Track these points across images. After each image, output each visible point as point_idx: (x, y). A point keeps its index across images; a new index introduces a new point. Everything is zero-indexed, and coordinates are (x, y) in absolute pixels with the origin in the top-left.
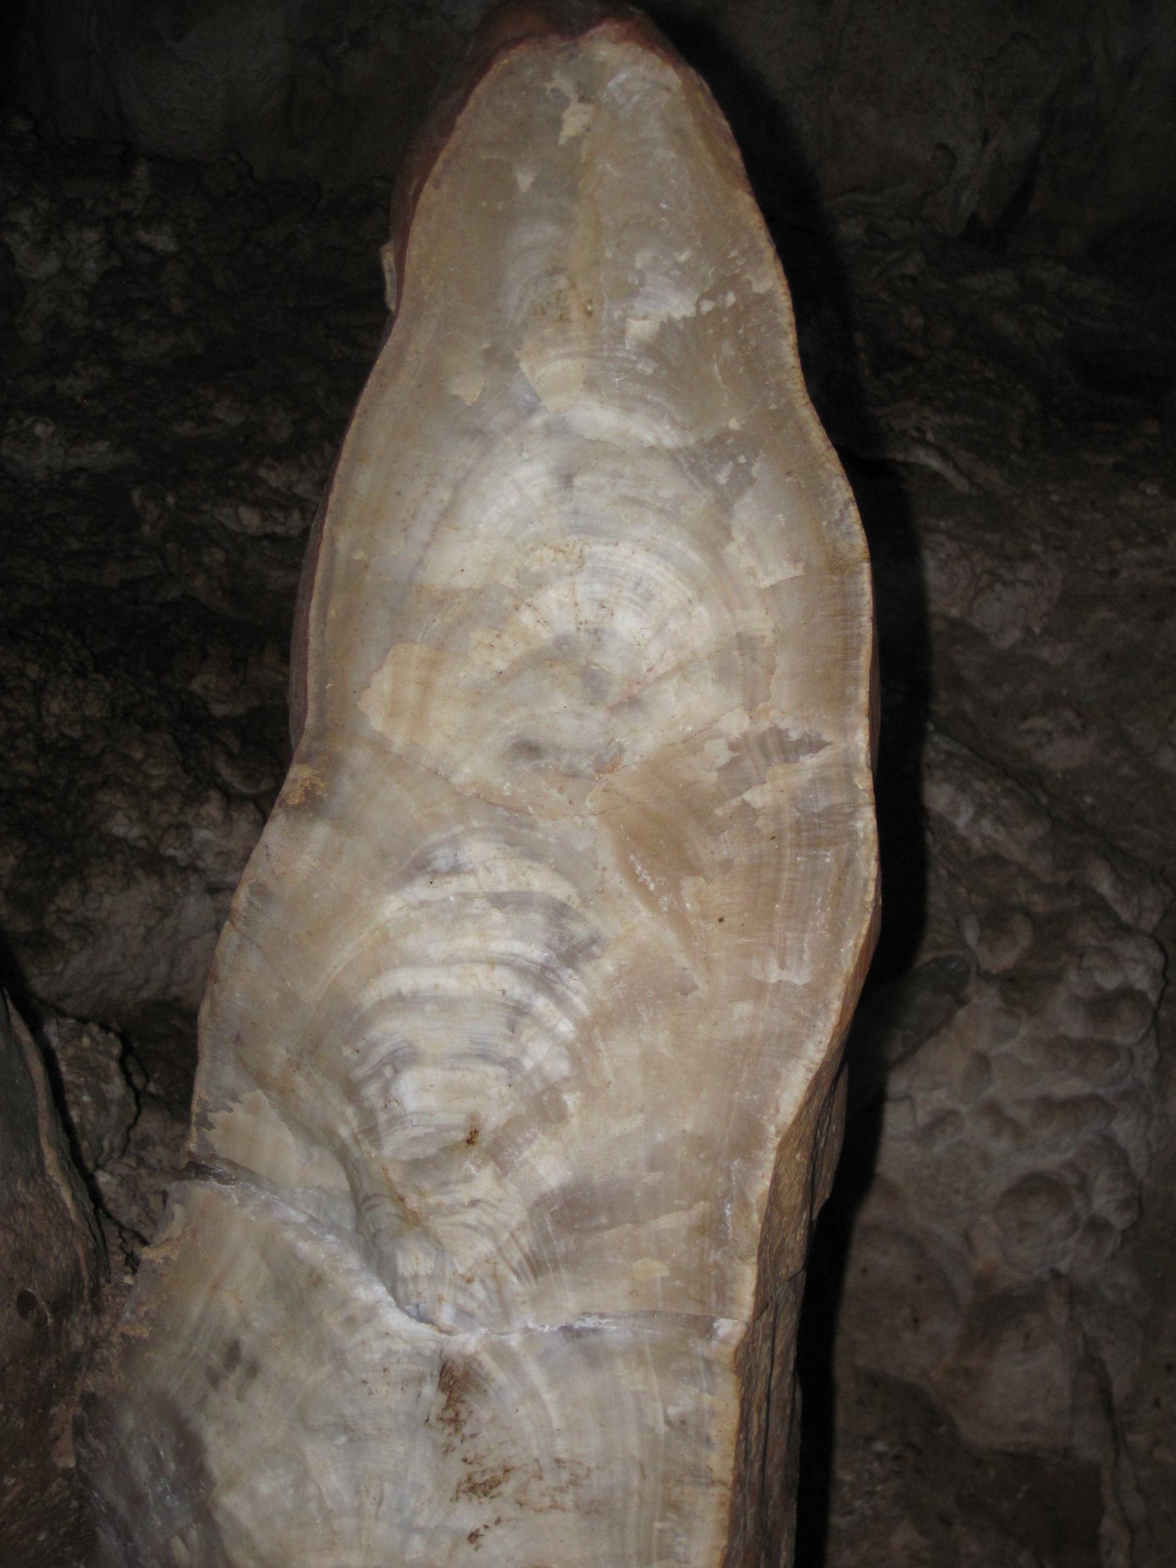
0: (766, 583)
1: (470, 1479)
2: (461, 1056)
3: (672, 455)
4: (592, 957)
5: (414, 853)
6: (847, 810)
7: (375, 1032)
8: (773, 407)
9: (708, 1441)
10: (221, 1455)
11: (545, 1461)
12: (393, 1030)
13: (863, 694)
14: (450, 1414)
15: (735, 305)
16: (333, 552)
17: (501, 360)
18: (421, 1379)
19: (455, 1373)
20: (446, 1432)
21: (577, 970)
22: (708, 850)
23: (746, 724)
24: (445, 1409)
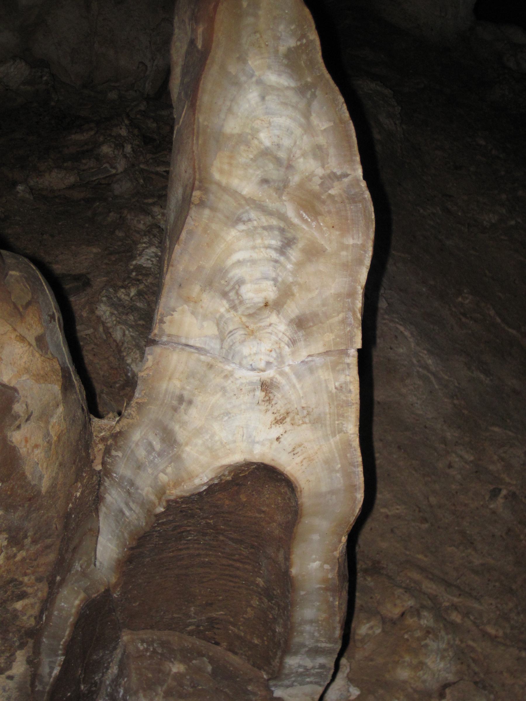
0: (323, 128)
1: (275, 419)
2: (258, 279)
3: (293, 89)
4: (295, 243)
5: (236, 216)
6: (361, 192)
7: (231, 275)
8: (318, 74)
9: (350, 391)
10: (181, 434)
11: (299, 408)
12: (236, 273)
13: (358, 158)
14: (267, 398)
15: (306, 43)
16: (199, 122)
17: (242, 59)
18: (254, 390)
19: (267, 384)
20: (266, 405)
21: (291, 248)
22: (323, 209)
23: (323, 172)
24: (265, 397)
